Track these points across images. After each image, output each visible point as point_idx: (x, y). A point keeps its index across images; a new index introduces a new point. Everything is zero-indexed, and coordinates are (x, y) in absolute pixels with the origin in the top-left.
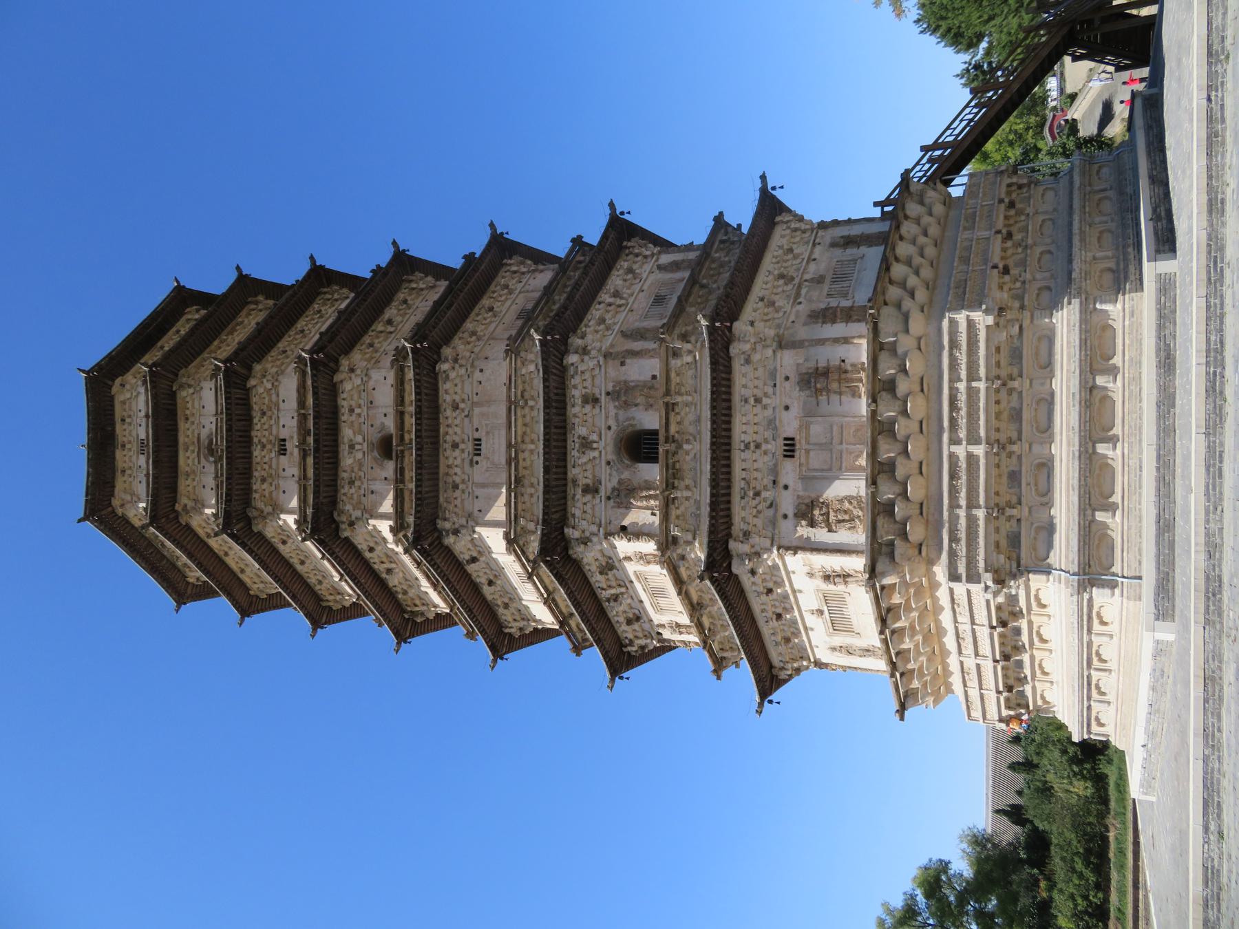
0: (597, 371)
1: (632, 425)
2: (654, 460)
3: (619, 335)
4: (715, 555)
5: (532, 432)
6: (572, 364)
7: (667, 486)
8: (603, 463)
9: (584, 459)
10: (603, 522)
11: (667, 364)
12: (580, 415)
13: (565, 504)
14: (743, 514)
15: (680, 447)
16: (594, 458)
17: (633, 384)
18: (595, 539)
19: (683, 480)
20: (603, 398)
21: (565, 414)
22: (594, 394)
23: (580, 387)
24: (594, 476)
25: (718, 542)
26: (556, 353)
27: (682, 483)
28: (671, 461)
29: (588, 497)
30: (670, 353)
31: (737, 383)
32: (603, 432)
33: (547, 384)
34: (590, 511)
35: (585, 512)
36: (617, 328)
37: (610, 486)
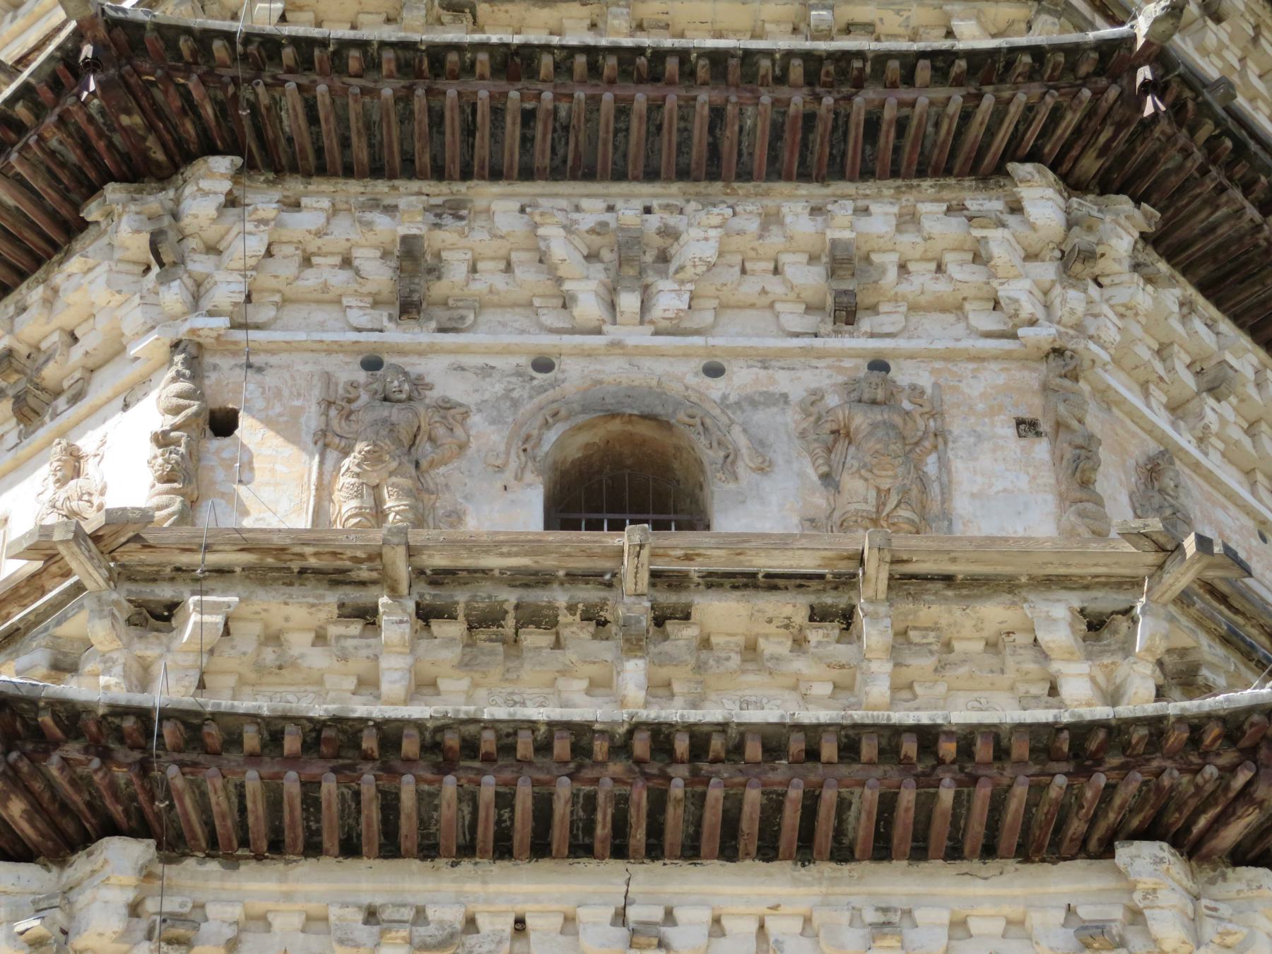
0: (990, 322)
1: (730, 459)
3: (1153, 447)
4: (73, 750)
6: (1016, 208)
7: (440, 577)
8: (546, 342)
9: (560, 249)
10: (254, 335)
11: (1050, 583)
12: (775, 240)
13: (349, 172)
14: (286, 921)
15: (634, 645)
16: (566, 303)
17: (931, 466)
18: (173, 296)
19: (465, 665)
21: (776, 172)
22: (873, 309)
23: (907, 240)
24: (480, 306)
25: (144, 768)
26: (1071, 119)
27: (452, 654)
28: (560, 597)
29: (379, 275)
30: (1105, 601)
31: (977, 889)
32: (698, 341)
33: (924, 71)
34: (311, 279)
35: (307, 261)
36: (1185, 441)
37: (433, 368)
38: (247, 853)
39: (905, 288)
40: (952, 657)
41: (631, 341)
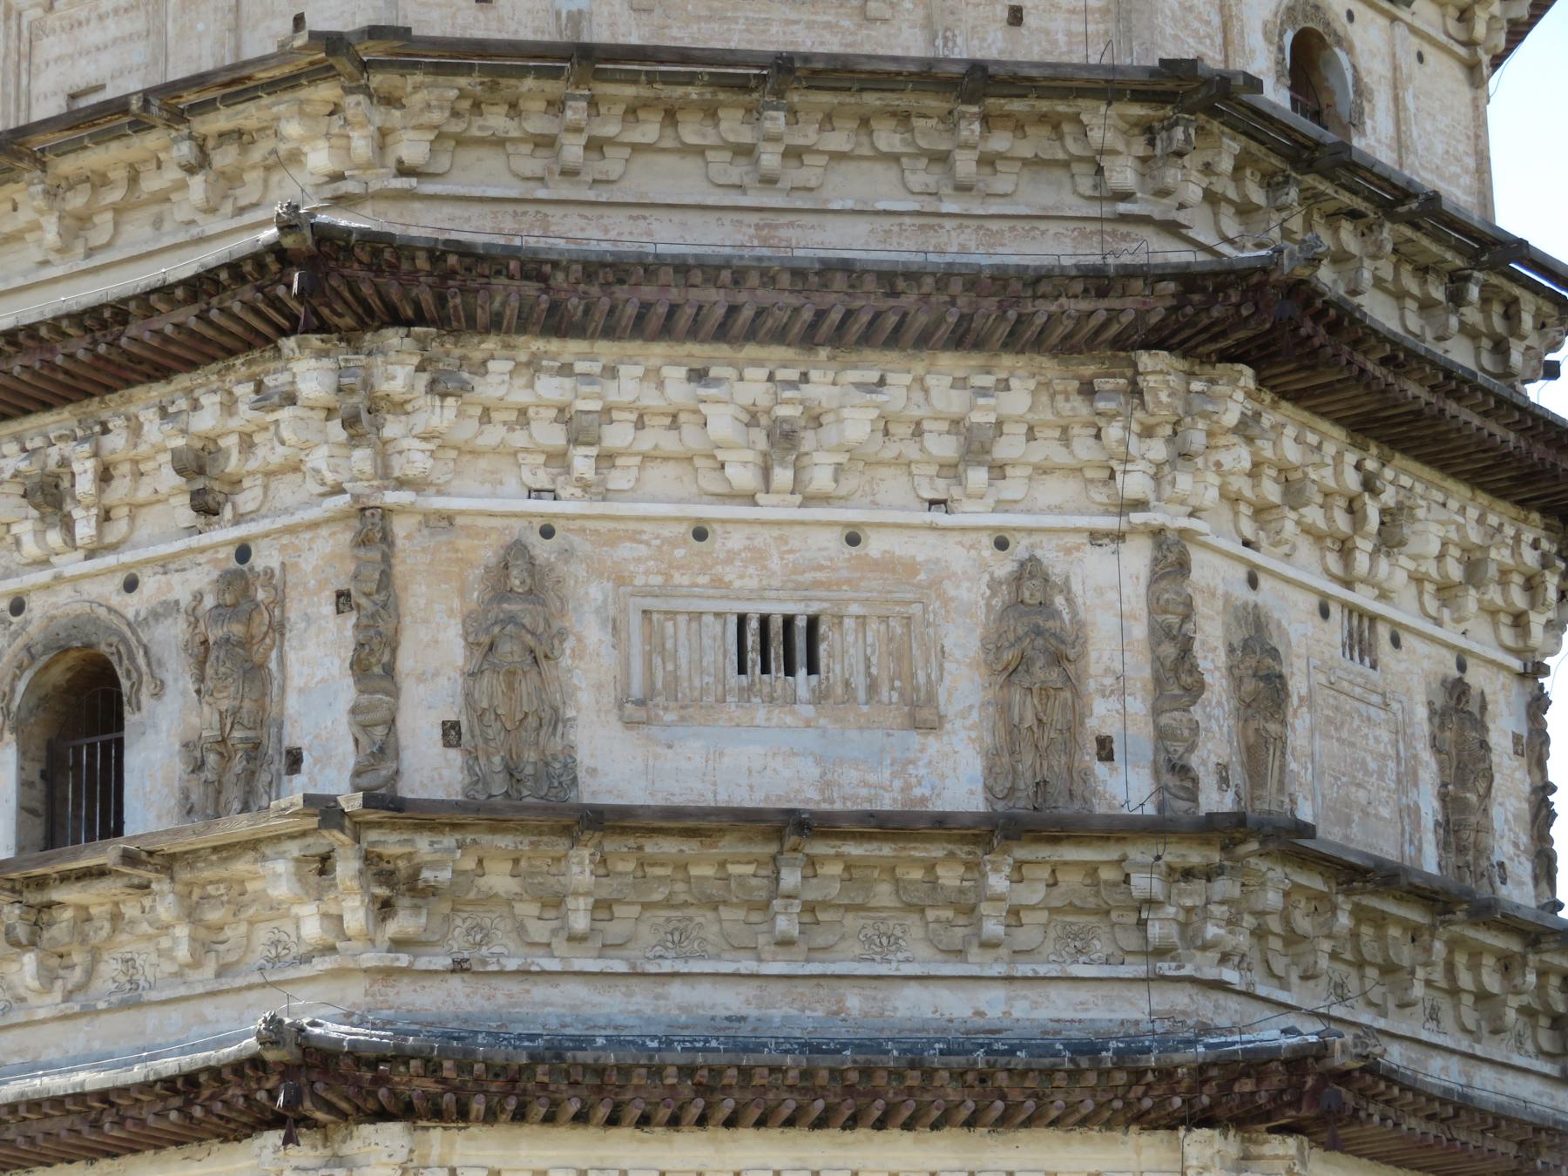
2: (365, 806)
5: (118, 210)
20: (224, 534)
32: (110, 560)
38: (274, 654)
39: (253, 464)
40: (246, 898)
41: (69, 571)
